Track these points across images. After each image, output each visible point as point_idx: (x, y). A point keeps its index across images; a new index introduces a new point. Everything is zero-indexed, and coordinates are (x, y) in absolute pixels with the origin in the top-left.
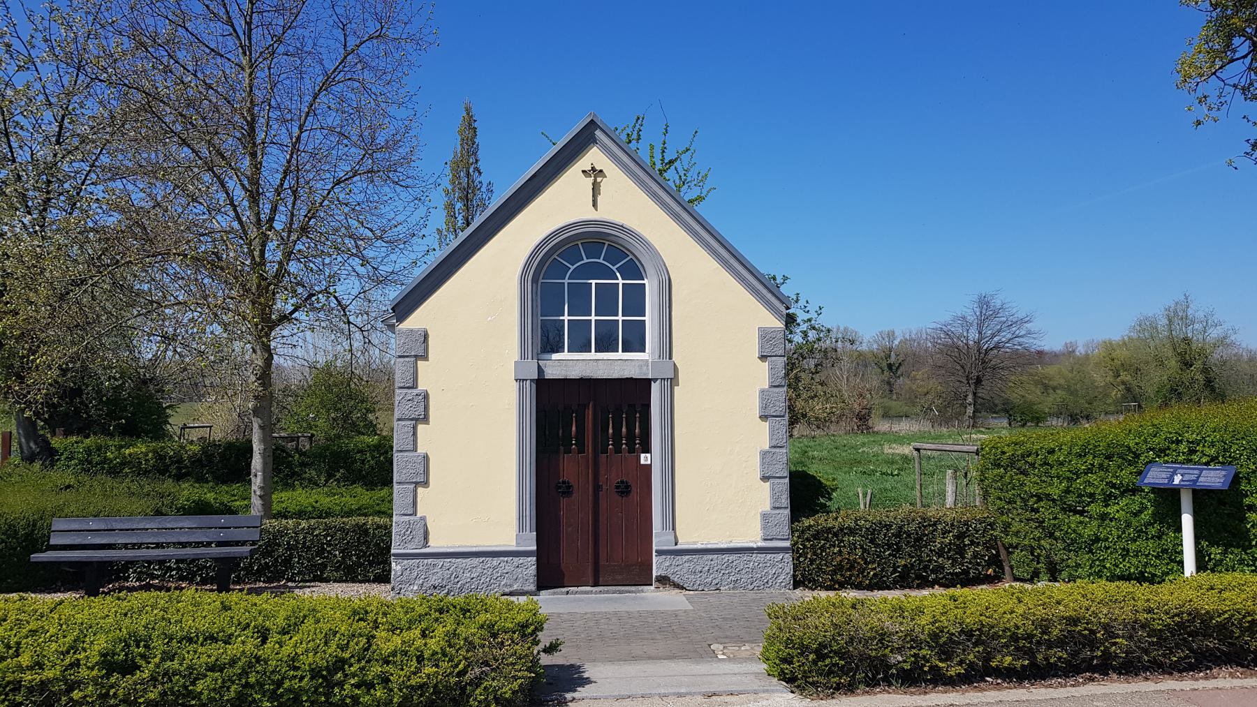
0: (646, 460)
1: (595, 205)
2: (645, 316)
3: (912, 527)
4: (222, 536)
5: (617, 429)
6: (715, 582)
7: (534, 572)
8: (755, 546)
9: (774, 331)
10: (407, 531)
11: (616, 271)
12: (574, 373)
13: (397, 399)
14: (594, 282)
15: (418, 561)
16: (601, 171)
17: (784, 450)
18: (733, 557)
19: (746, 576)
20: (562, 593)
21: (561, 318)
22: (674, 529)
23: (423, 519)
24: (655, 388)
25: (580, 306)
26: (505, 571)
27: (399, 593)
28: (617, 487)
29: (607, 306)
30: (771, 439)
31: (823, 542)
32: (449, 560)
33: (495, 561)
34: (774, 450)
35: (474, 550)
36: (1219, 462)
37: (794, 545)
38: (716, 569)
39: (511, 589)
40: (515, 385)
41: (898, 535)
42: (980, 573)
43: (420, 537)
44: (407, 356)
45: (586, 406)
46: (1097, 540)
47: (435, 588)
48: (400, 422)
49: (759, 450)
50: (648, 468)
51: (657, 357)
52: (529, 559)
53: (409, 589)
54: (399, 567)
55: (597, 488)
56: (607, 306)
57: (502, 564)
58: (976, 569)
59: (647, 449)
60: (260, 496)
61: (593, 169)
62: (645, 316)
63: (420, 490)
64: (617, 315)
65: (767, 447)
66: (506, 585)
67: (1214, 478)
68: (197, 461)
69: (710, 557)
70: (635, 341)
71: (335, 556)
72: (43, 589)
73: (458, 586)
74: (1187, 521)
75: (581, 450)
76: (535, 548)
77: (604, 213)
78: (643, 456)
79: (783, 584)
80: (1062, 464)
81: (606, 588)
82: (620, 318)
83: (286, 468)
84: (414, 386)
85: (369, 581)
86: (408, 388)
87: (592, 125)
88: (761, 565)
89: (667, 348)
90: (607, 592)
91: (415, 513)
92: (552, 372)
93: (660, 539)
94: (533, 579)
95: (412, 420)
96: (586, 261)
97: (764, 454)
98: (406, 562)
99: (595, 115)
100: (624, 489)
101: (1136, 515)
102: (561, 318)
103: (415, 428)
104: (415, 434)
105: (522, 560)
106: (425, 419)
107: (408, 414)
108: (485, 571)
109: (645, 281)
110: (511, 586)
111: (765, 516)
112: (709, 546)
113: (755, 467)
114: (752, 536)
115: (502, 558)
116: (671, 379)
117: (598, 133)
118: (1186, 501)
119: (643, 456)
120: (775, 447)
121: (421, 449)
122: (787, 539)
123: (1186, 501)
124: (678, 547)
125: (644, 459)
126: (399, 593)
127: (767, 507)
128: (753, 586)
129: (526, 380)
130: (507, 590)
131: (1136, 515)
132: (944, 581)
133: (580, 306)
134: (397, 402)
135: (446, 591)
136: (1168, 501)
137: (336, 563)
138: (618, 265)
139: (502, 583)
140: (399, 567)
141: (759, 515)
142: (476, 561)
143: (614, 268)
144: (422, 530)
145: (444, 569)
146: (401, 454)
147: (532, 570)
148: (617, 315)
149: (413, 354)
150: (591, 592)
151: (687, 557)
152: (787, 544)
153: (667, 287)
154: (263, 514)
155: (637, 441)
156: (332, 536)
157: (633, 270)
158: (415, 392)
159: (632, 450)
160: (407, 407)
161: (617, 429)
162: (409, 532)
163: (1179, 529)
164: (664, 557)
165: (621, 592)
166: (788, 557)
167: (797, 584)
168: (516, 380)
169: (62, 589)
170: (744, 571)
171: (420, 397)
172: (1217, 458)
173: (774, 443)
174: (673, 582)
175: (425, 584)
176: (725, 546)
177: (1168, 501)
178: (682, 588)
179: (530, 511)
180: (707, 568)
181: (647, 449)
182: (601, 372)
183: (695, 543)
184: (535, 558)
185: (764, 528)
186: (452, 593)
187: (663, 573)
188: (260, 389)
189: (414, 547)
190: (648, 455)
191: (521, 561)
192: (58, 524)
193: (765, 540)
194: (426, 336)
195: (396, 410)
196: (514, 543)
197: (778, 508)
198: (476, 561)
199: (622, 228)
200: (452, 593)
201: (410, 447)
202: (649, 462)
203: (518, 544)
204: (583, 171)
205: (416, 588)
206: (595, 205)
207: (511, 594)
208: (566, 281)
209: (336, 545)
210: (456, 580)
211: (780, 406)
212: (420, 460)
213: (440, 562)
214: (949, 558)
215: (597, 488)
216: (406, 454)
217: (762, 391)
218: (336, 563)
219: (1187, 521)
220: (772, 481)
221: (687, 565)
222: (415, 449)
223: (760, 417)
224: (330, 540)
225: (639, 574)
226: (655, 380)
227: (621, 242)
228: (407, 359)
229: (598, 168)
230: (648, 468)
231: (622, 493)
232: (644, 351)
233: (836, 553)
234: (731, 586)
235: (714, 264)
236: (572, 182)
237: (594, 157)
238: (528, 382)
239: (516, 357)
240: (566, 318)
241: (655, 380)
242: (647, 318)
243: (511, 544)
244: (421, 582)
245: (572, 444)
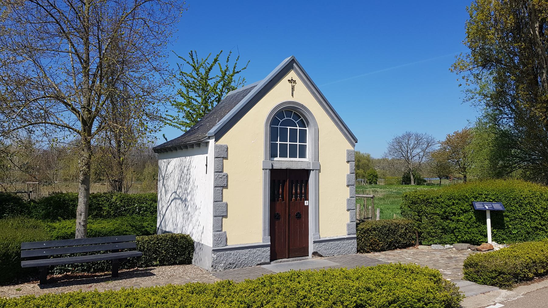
0: (307, 204)
1: (292, 95)
2: (306, 143)
3: (393, 227)
4: (112, 247)
5: (301, 190)
6: (333, 253)
7: (270, 254)
8: (346, 237)
10: (219, 238)
12: (284, 167)
14: (289, 128)
15: (223, 252)
18: (338, 242)
20: (279, 262)
21: (277, 142)
25: (284, 139)
26: (259, 254)
27: (215, 268)
28: (297, 215)
29: (293, 139)
30: (350, 194)
31: (367, 234)
32: (236, 251)
33: (255, 250)
34: (351, 199)
35: (247, 245)
36: (495, 201)
37: (357, 236)
38: (333, 247)
39: (261, 262)
40: (262, 172)
41: (388, 230)
42: (411, 243)
43: (224, 242)
44: (219, 157)
45: (284, 182)
46: (456, 228)
47: (230, 264)
48: (216, 188)
49: (346, 199)
51: (314, 160)
52: (268, 248)
53: (220, 266)
54: (215, 256)
56: (293, 139)
57: (257, 251)
58: (410, 241)
60: (83, 225)
62: (306, 143)
63: (224, 219)
64: (287, 142)
65: (349, 198)
66: (259, 261)
67: (497, 206)
69: (331, 243)
71: (162, 253)
72: (9, 283)
73: (240, 263)
74: (489, 221)
76: (270, 243)
77: (296, 99)
78: (305, 201)
80: (443, 202)
81: (294, 259)
82: (298, 143)
83: (26, 210)
85: (177, 264)
86: (220, 172)
87: (293, 61)
90: (295, 260)
91: (221, 231)
92: (276, 166)
94: (269, 257)
95: (221, 187)
97: (348, 200)
98: (218, 253)
99: (294, 57)
100: (299, 216)
101: (469, 219)
102: (277, 142)
105: (265, 249)
106: (226, 187)
108: (251, 255)
109: (307, 129)
110: (261, 261)
111: (348, 225)
112: (331, 238)
115: (257, 249)
117: (294, 65)
118: (488, 214)
119: (305, 201)
120: (351, 197)
122: (355, 234)
123: (488, 214)
124: (321, 239)
126: (215, 268)
127: (348, 221)
129: (267, 169)
130: (259, 263)
131: (469, 219)
132: (400, 246)
133: (284, 139)
135: (235, 265)
136: (481, 215)
137: (162, 256)
138: (295, 121)
139: (258, 260)
140: (215, 256)
141: (346, 225)
142: (247, 250)
143: (296, 122)
145: (234, 255)
146: (216, 203)
147: (269, 253)
148: (287, 142)
149: (222, 156)
150: (289, 261)
151: (324, 243)
152: (355, 236)
153: (317, 132)
154: (84, 234)
155: (303, 196)
156: (161, 244)
158: (223, 174)
160: (219, 181)
161: (301, 190)
162: (220, 239)
163: (485, 223)
164: (316, 244)
165: (300, 260)
166: (355, 241)
167: (358, 251)
168: (263, 169)
169: (20, 282)
170: (342, 248)
171: (225, 177)
172: (495, 200)
173: (351, 196)
174: (319, 254)
175: (226, 263)
176: (336, 238)
177: (481, 215)
178: (321, 256)
182: (294, 166)
183: (326, 237)
184: (270, 248)
185: (348, 230)
186: (237, 266)
187: (315, 250)
188: (87, 170)
189: (222, 246)
190: (307, 201)
191: (264, 249)
193: (348, 234)
194: (227, 148)
196: (261, 241)
197: (352, 222)
198: (247, 251)
199: (302, 106)
200: (237, 266)
201: (220, 199)
202: (308, 204)
203: (263, 242)
204: (289, 80)
205: (222, 265)
206: (292, 95)
207: (260, 264)
208: (279, 126)
209: (163, 248)
210: (239, 260)
211: (353, 181)
212: (224, 205)
213: (232, 252)
214: (402, 238)
216: (218, 203)
218: (162, 256)
219: (489, 221)
220: (350, 211)
221: (323, 246)
224: (160, 246)
225: (303, 252)
226: (313, 170)
227: (301, 111)
228: (219, 159)
231: (299, 217)
233: (373, 237)
235: (333, 123)
236: (283, 85)
237: (292, 75)
238: (268, 170)
240: (278, 142)
241: (313, 170)
242: (307, 144)
243: (261, 242)
245: (280, 197)
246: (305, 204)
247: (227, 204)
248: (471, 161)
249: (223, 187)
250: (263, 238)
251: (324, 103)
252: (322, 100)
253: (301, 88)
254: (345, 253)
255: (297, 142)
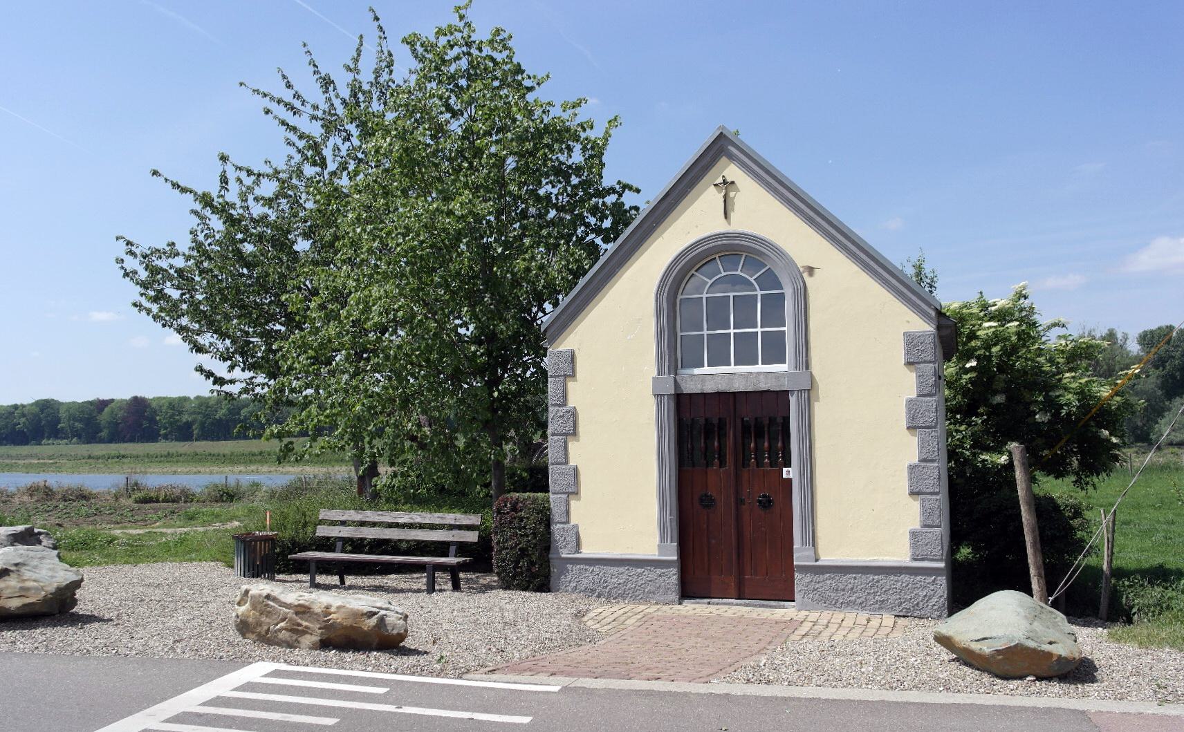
1: (726, 215)
9: (923, 335)
11: (754, 282)
13: (551, 415)
16: (733, 183)
17: (936, 464)
19: (894, 597)
22: (814, 545)
23: (576, 526)
24: (793, 400)
30: (920, 452)
34: (923, 464)
40: (652, 403)
50: (790, 480)
55: (739, 502)
57: (646, 572)
59: (788, 464)
61: (725, 182)
68: (78, 621)
70: (775, 351)
75: (722, 463)
76: (675, 558)
78: (785, 470)
79: (935, 607)
81: (747, 601)
82: (759, 330)
84: (564, 404)
86: (559, 405)
88: (909, 586)
89: (804, 361)
91: (568, 522)
92: (690, 387)
93: (801, 556)
96: (724, 274)
100: (766, 503)
103: (566, 443)
104: (566, 448)
107: (560, 430)
111: (914, 534)
113: (903, 483)
114: (901, 555)
116: (809, 390)
119: (785, 470)
121: (572, 463)
125: (786, 473)
128: (901, 608)
134: (550, 420)
144: (574, 538)
148: (762, 332)
152: (942, 565)
157: (770, 280)
158: (565, 408)
159: (773, 463)
168: (655, 395)
170: (891, 592)
175: (578, 587)
179: (671, 518)
180: (850, 586)
181: (788, 464)
192: (324, 514)
195: (550, 425)
196: (657, 554)
201: (564, 461)
210: (605, 585)
215: (739, 502)
217: (910, 401)
221: (828, 582)
222: (566, 463)
223: (908, 428)
229: (729, 180)
230: (790, 480)
232: (784, 362)
234: (877, 606)
238: (666, 397)
239: (655, 373)
244: (574, 585)
246: (785, 476)
247: (576, 470)
248: (859, 641)
249: (566, 434)
250: (507, 584)
251: (818, 219)
252: (811, 214)
253: (749, 192)
254: (903, 606)
255: (762, 332)
